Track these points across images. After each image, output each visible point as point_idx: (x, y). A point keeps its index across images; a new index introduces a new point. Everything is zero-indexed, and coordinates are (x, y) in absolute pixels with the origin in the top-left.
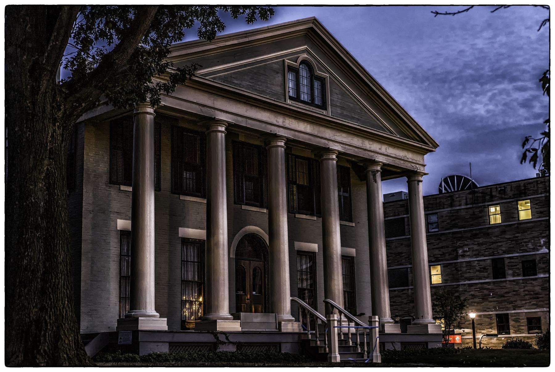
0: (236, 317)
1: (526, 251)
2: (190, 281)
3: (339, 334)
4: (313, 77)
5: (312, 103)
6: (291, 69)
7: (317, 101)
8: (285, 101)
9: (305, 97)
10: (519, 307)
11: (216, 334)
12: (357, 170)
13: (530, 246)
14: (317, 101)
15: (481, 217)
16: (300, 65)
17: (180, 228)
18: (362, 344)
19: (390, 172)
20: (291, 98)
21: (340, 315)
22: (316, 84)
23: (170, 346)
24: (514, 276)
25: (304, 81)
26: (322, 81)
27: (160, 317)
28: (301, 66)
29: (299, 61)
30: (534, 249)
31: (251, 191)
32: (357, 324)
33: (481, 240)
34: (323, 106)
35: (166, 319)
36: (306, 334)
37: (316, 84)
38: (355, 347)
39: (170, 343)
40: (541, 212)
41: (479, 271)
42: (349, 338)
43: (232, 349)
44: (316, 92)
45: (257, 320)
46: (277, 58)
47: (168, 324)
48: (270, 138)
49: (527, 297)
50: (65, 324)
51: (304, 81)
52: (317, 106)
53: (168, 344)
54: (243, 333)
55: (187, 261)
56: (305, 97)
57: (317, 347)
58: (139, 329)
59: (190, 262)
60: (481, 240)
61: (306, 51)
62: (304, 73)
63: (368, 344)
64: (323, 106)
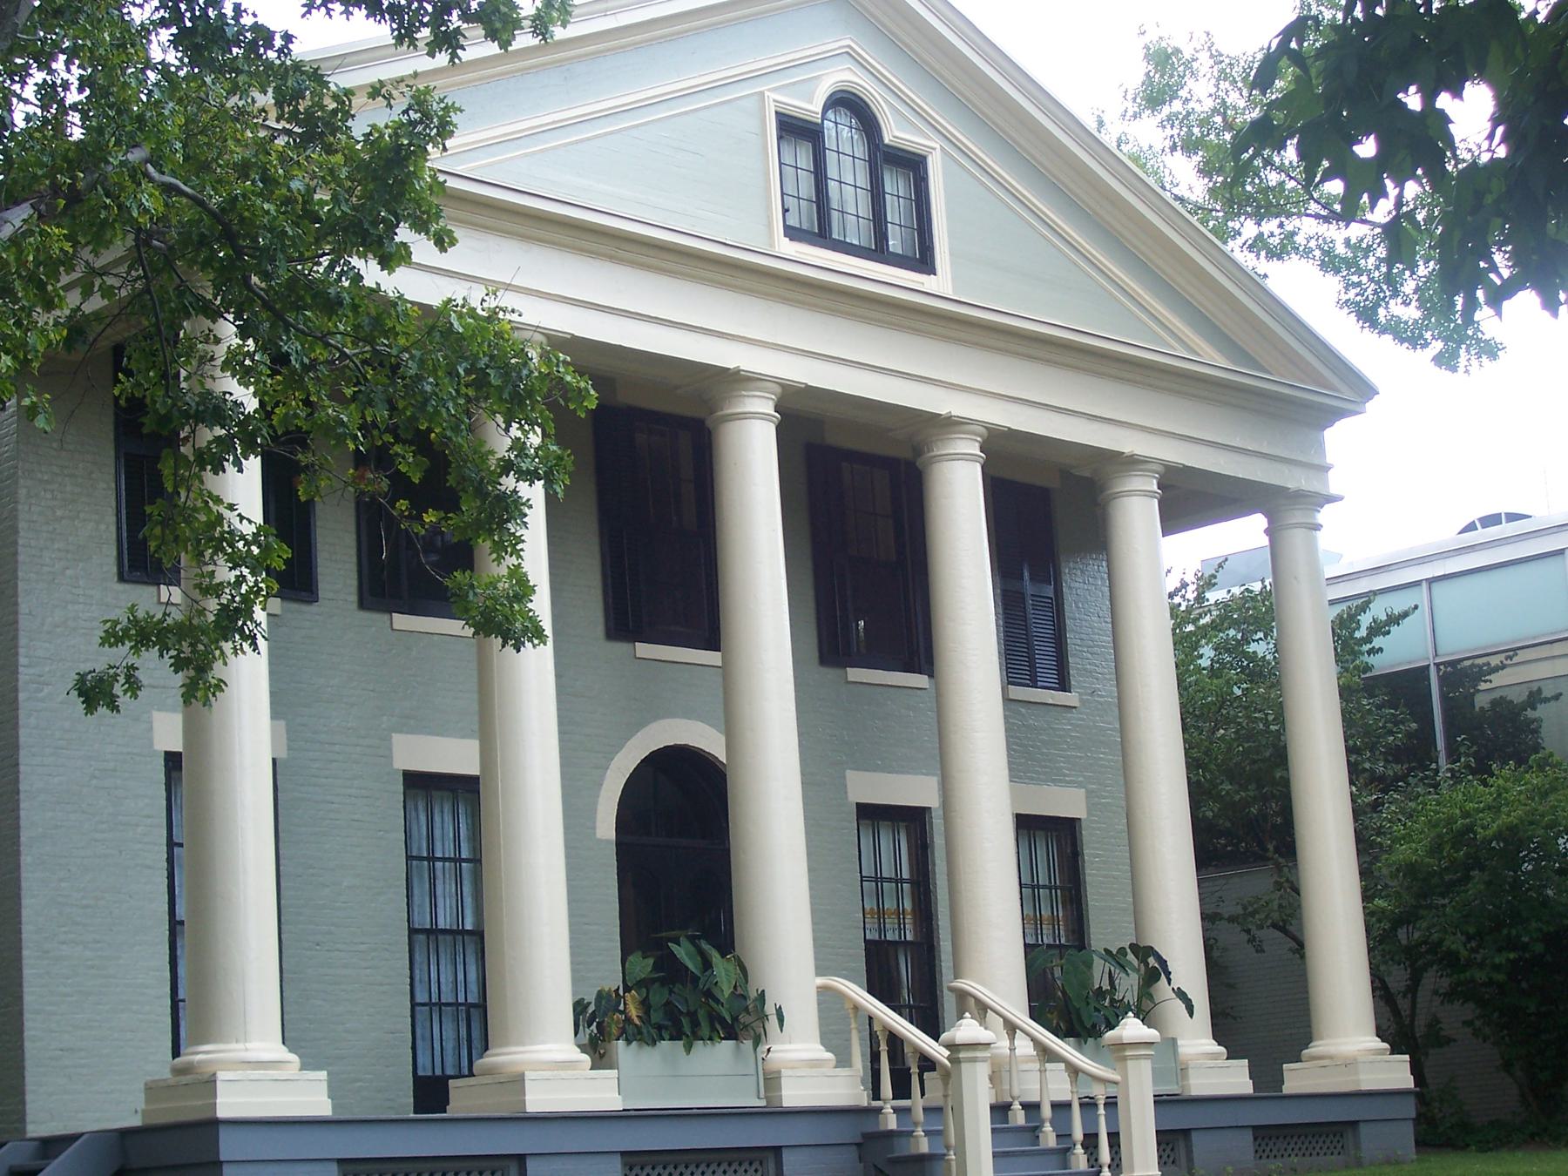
2: (445, 931)
3: (1000, 1110)
5: (878, 251)
8: (772, 245)
15: (154, 527)
16: (825, 109)
18: (1090, 1142)
19: (1189, 499)
21: (1012, 1037)
23: (624, 1164)
26: (913, 165)
27: (303, 1067)
28: (830, 114)
31: (657, 579)
32: (1074, 1071)
34: (923, 261)
35: (1407, 1057)
36: (879, 1110)
38: (1064, 1153)
39: (1254, 1128)
42: (1043, 1122)
47: (1416, 1069)
48: (717, 385)
53: (618, 1160)
56: (856, 230)
58: (222, 1113)
59: (444, 859)
62: (841, 135)
63: (1114, 1137)
64: (923, 261)
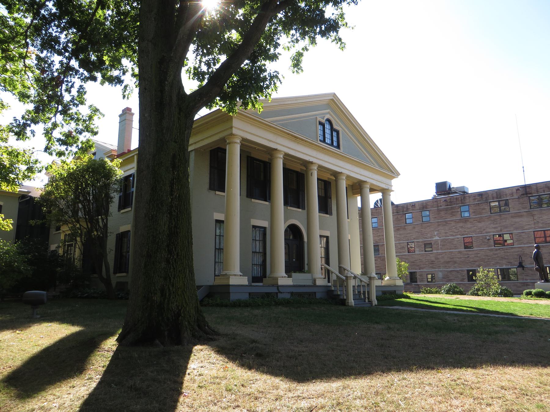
0: (290, 276)
1: (426, 238)
4: (332, 129)
5: (332, 144)
6: (321, 123)
7: (335, 144)
9: (328, 141)
10: (422, 268)
11: (278, 287)
12: (357, 187)
13: (429, 235)
14: (335, 144)
17: (252, 220)
20: (320, 141)
22: (335, 134)
24: (420, 251)
25: (328, 131)
29: (325, 118)
30: (431, 237)
33: (401, 232)
34: (338, 147)
37: (335, 134)
40: (435, 218)
41: (400, 249)
43: (288, 296)
44: (335, 139)
45: (299, 278)
46: (313, 115)
49: (427, 263)
50: (186, 292)
51: (328, 131)
52: (335, 147)
54: (294, 286)
55: (256, 240)
56: (328, 141)
57: (339, 295)
60: (401, 232)
61: (329, 113)
62: (327, 126)
